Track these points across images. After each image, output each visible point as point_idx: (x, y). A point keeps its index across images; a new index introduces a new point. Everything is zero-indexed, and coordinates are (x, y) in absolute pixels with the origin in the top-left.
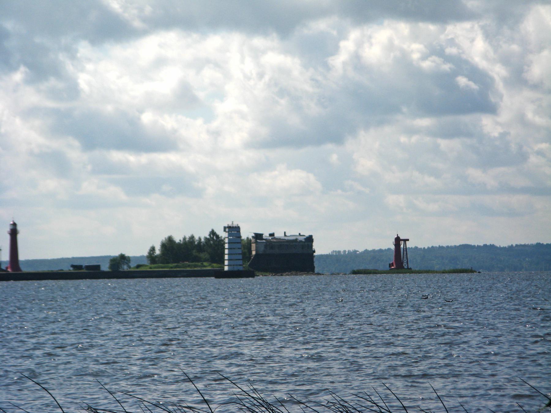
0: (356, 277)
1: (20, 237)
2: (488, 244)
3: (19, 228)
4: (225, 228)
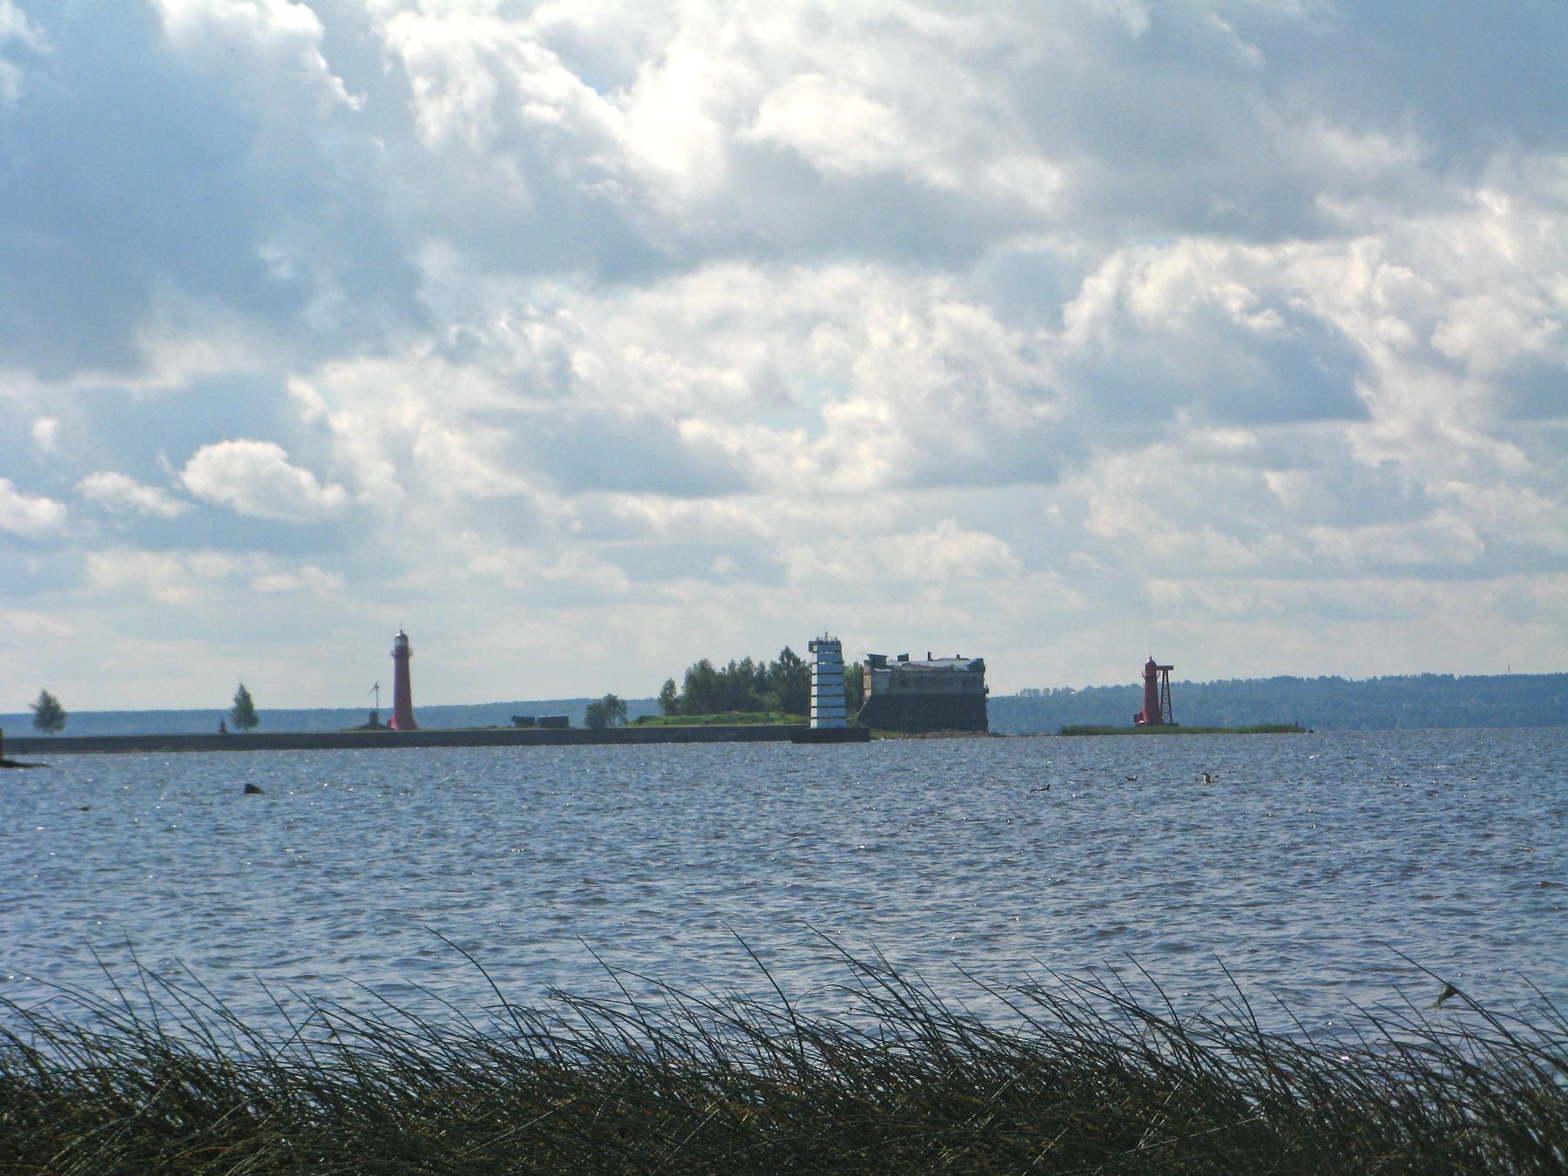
0: (1070, 740)
1: (413, 663)
2: (1329, 676)
3: (411, 644)
4: (811, 645)
